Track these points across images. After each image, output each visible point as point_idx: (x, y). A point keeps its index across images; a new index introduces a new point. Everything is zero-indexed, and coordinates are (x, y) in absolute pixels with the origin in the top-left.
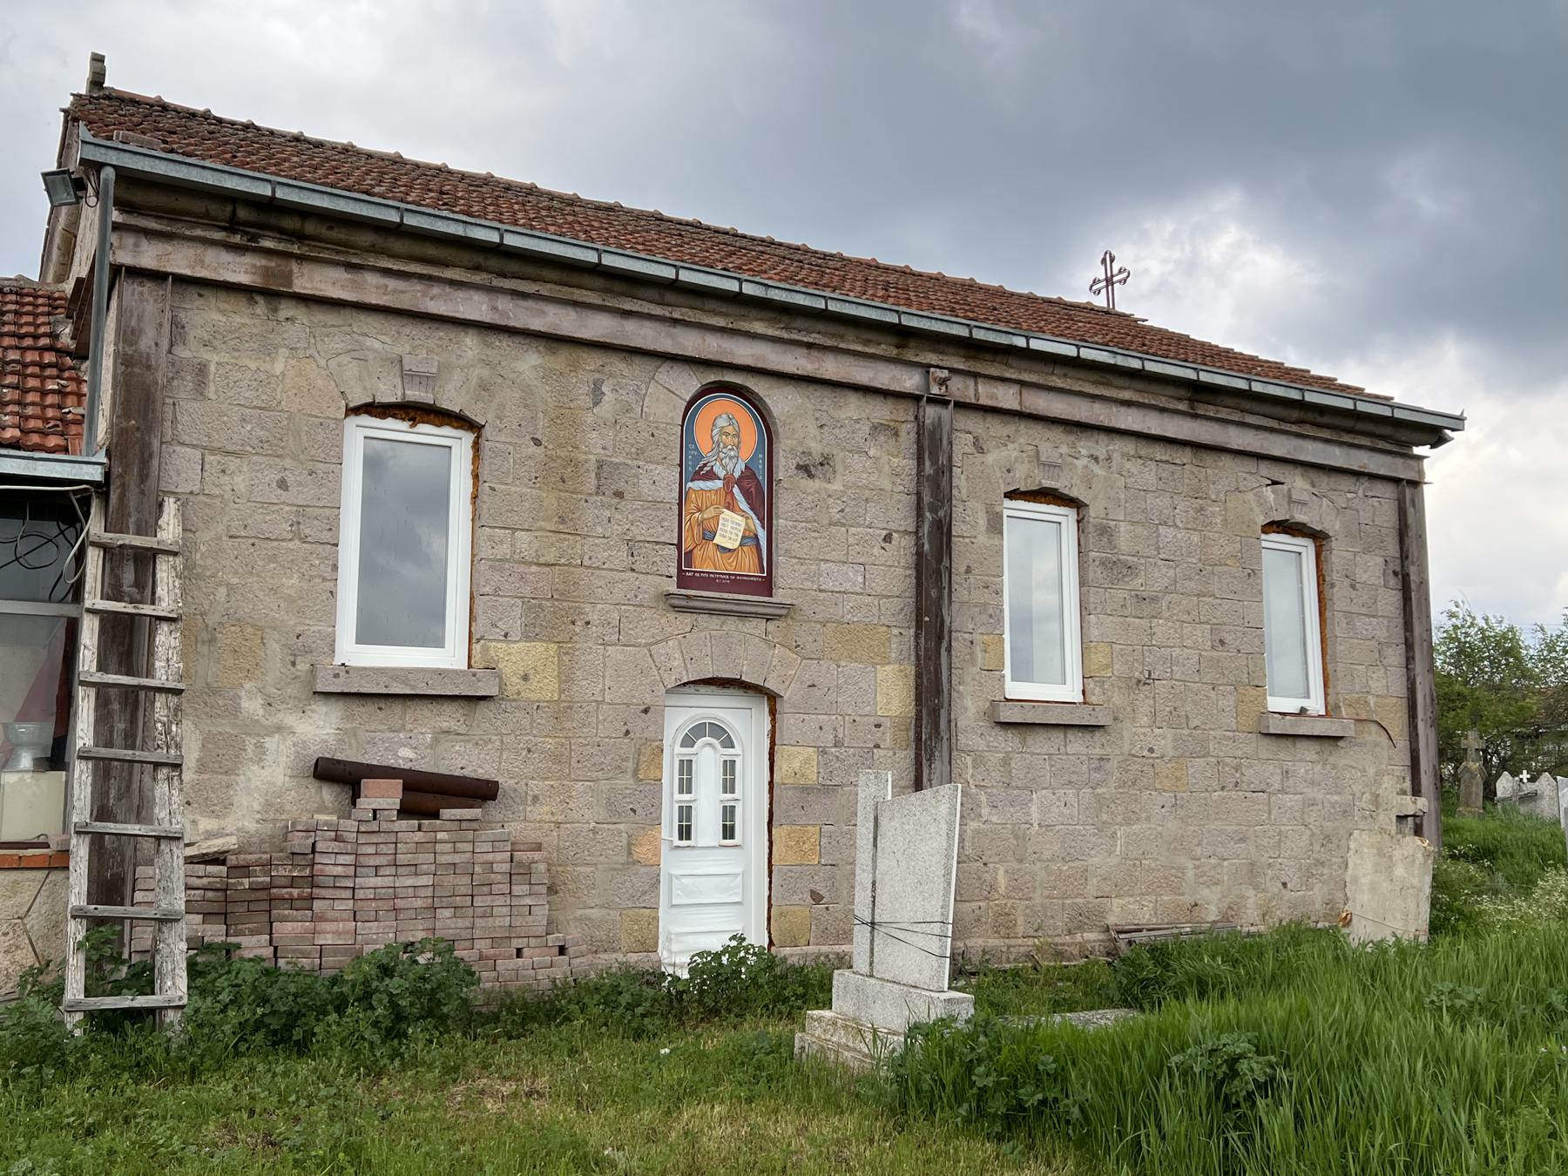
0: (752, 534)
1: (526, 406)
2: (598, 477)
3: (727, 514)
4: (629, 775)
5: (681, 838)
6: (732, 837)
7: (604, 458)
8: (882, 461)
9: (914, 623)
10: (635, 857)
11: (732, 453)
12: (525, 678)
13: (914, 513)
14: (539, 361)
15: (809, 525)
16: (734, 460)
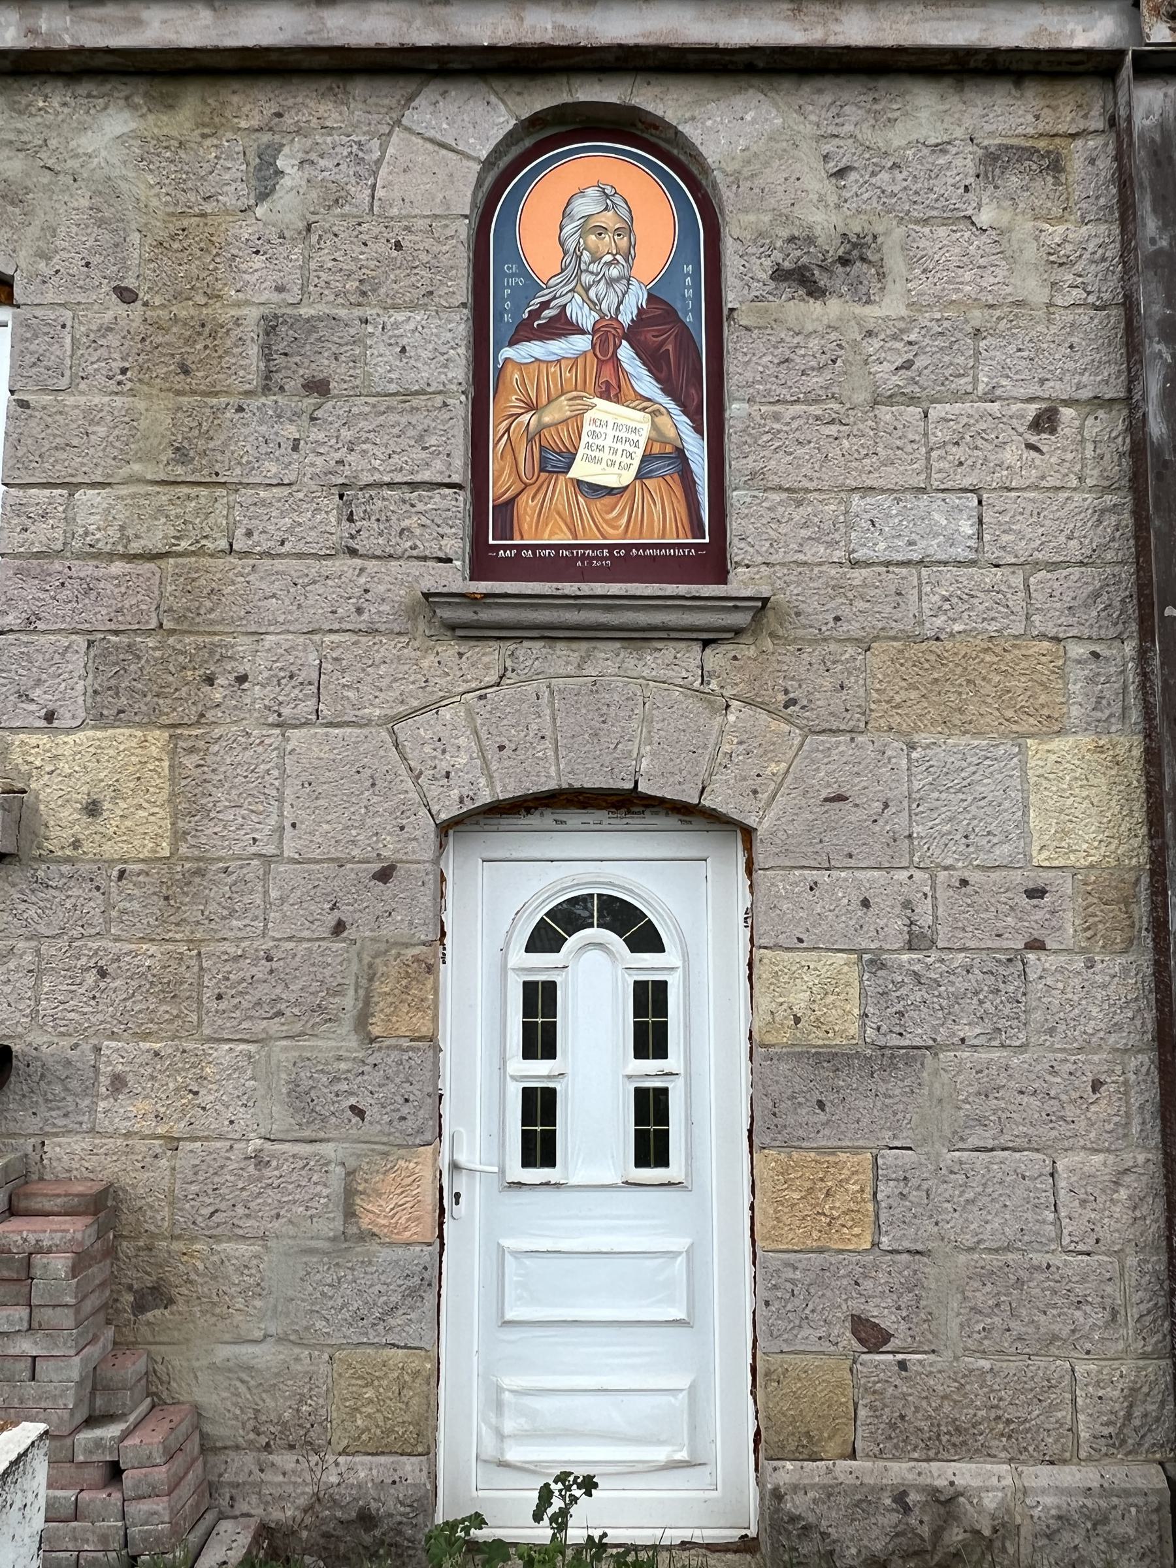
0: (669, 449)
1: (101, 223)
2: (267, 353)
3: (604, 409)
4: (346, 1027)
5: (527, 1162)
6: (662, 1160)
7: (279, 312)
8: (1016, 236)
9: (1134, 627)
10: (365, 1222)
11: (614, 272)
12: (93, 809)
13: (1119, 353)
14: (133, 125)
15: (816, 410)
16: (620, 287)
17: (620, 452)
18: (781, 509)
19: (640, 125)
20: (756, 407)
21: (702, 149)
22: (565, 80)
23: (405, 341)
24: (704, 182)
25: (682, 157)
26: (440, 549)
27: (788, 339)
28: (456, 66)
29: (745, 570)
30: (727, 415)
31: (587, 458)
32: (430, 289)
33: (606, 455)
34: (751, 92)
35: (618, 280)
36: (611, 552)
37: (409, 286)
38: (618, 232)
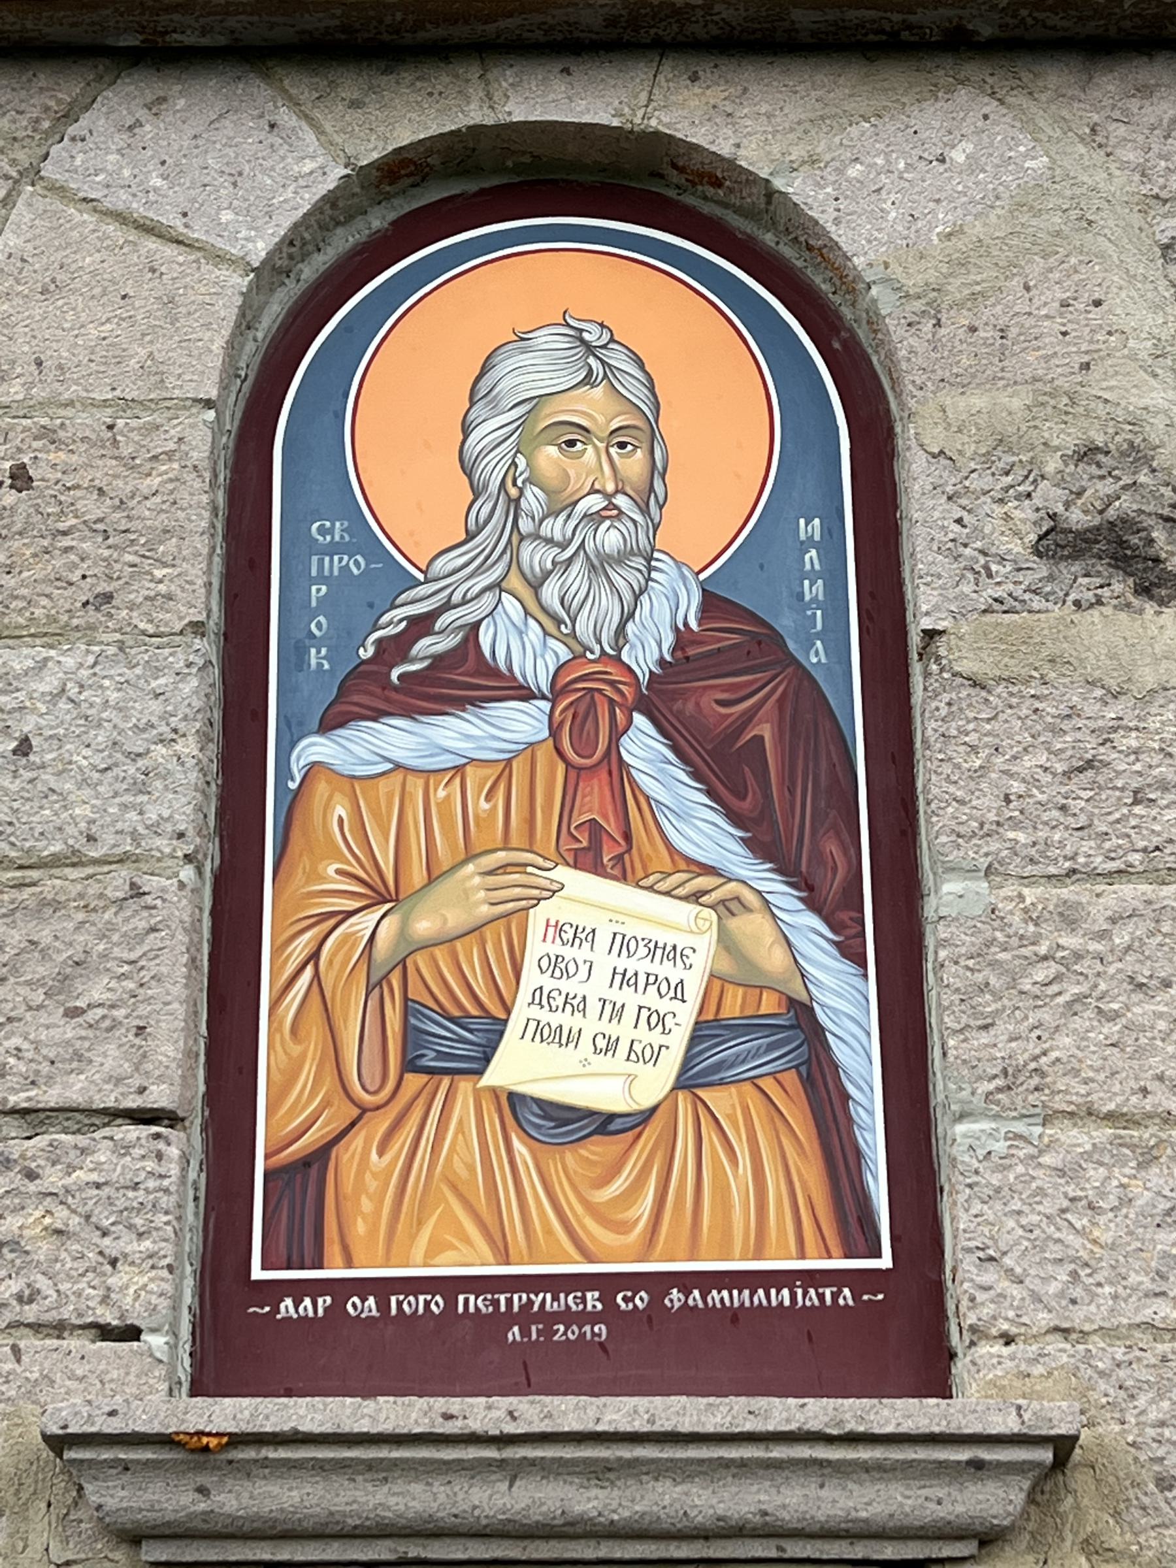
0: (769, 1004)
11: (610, 539)
16: (625, 578)
17: (630, 1014)
18: (1096, 1174)
19: (675, 177)
20: (1010, 890)
21: (841, 236)
22: (474, 72)
23: (28, 725)
24: (847, 312)
25: (787, 251)
26: (105, 1300)
27: (1091, 709)
28: (189, 39)
29: (998, 1348)
30: (931, 908)
31: (539, 1032)
32: (104, 587)
33: (591, 1025)
34: (963, 94)
35: (620, 559)
36: (607, 1299)
37: (46, 580)
38: (619, 439)
